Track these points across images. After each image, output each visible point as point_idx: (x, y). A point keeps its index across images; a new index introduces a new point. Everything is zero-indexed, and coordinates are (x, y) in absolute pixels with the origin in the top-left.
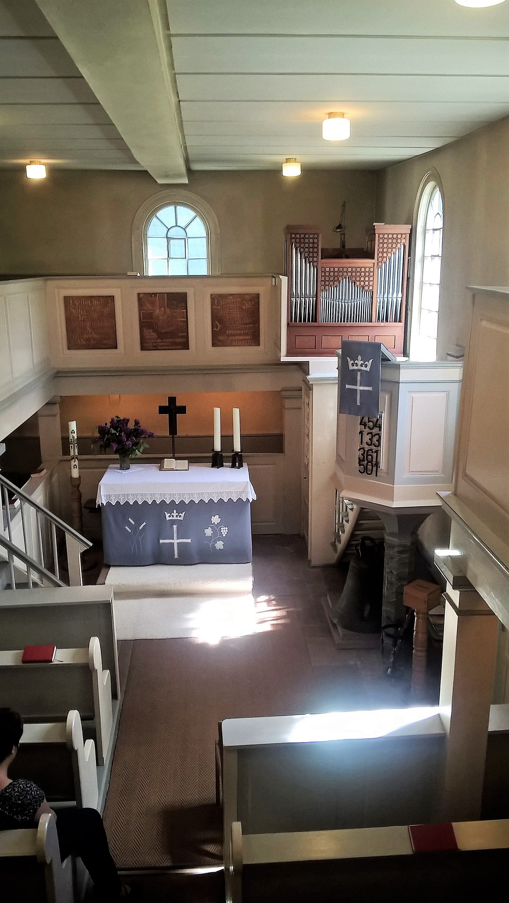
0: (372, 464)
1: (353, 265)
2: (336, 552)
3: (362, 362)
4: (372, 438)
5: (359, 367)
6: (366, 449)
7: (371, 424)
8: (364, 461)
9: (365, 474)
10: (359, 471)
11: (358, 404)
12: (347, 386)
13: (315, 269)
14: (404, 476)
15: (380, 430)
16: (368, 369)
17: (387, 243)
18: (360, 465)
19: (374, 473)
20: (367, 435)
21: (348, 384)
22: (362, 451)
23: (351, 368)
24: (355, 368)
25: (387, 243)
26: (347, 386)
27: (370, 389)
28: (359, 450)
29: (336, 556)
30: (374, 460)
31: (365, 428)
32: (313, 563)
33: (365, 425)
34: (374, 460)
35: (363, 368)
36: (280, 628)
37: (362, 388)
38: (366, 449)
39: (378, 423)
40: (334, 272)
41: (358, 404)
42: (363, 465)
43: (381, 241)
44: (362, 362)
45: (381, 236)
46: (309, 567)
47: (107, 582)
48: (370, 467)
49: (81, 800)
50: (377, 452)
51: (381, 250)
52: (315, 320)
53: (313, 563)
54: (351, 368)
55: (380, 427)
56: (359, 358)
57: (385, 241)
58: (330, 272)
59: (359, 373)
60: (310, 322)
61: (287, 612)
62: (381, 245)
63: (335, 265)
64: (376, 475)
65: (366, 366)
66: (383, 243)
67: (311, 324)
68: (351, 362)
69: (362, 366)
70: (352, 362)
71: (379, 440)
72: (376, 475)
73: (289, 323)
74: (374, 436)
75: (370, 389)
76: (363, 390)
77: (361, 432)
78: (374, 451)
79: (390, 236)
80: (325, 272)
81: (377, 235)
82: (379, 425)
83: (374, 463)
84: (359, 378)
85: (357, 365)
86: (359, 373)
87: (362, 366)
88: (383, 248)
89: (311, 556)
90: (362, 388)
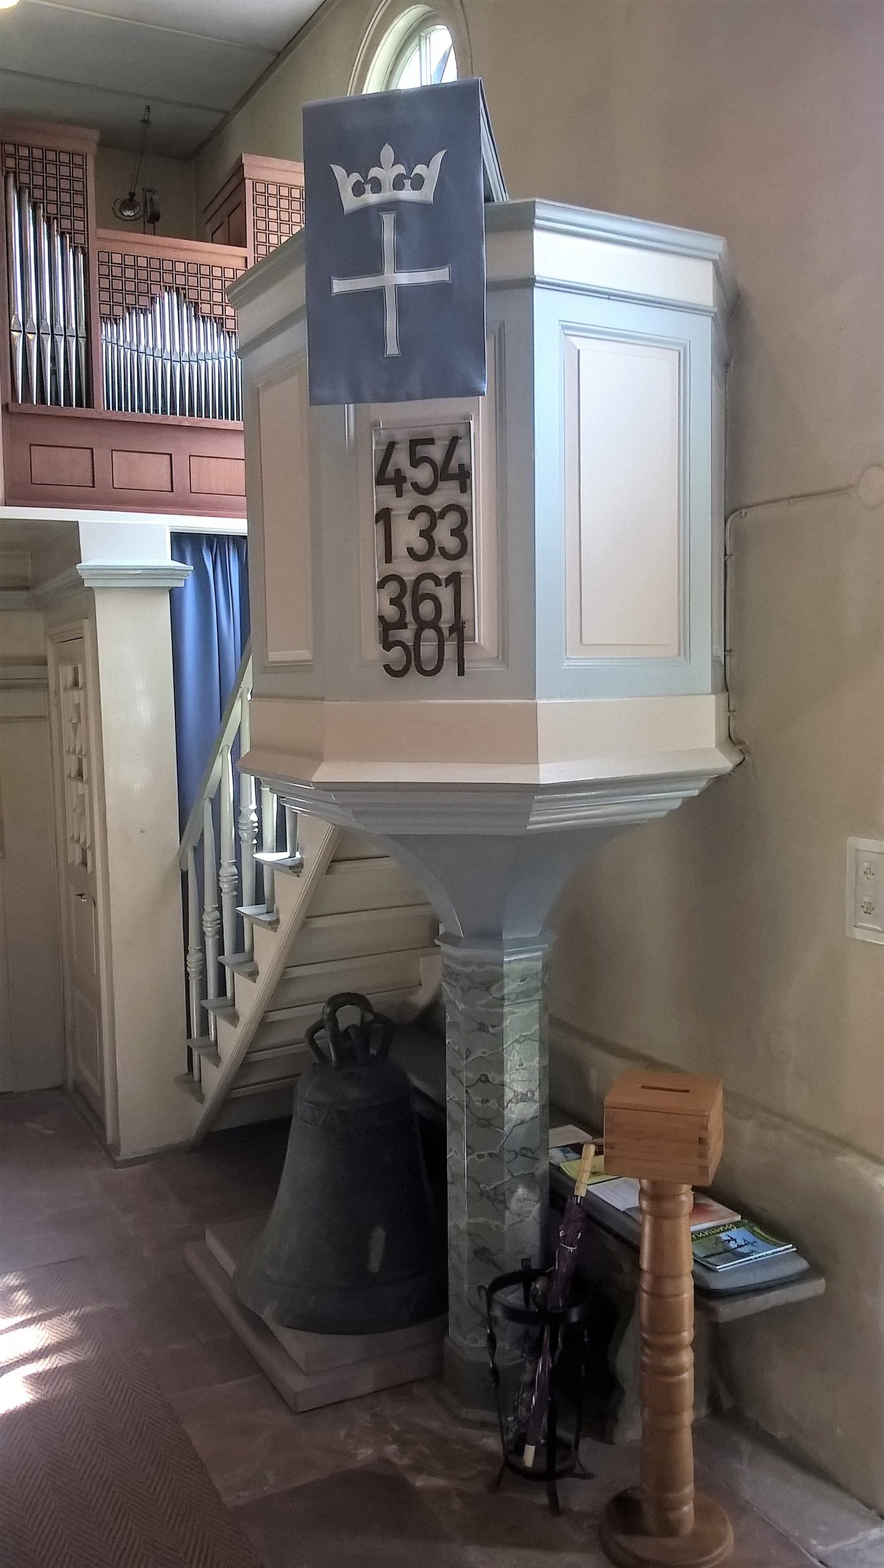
0: (439, 631)
1: (189, 257)
2: (201, 1100)
3: (401, 169)
4: (433, 525)
5: (388, 194)
6: (409, 579)
7: (423, 475)
8: (405, 626)
9: (413, 674)
10: (387, 668)
11: (392, 349)
12: (339, 286)
13: (81, 257)
14: (566, 662)
15: (465, 487)
16: (426, 194)
17: (278, 208)
18: (387, 645)
19: (450, 667)
20: (412, 516)
21: (344, 275)
22: (393, 588)
23: (350, 202)
24: (371, 198)
25: (278, 208)
26: (339, 286)
27: (442, 275)
28: (381, 585)
29: (199, 1113)
30: (447, 615)
31: (399, 494)
32: (126, 1152)
33: (398, 481)
34: (447, 615)
35: (407, 194)
36: (67, 1385)
37: (404, 278)
38: (409, 579)
39: (460, 453)
40: (136, 267)
41: (392, 349)
42: (399, 643)
43: (261, 200)
44: (401, 169)
45: (260, 188)
46: (116, 1165)
47: (618, 1439)
48: (428, 649)
49: (220, 814)
50: (455, 579)
51: (261, 225)
52: (87, 398)
53: (126, 1152)
54: (350, 202)
55: (463, 477)
56: (387, 153)
57: (272, 202)
58: (123, 266)
59: (388, 220)
60: (71, 405)
61: (75, 1319)
62: (261, 212)
63: (136, 250)
64: (461, 672)
65: (418, 183)
66: (267, 207)
67: (74, 410)
68: (345, 180)
69: (398, 184)
70: (356, 177)
71: (461, 532)
72: (461, 672)
73: (7, 405)
74: (442, 515)
75: (442, 275)
76: (409, 287)
77: (384, 516)
78: (442, 577)
79: (284, 192)
80: (110, 263)
81: (248, 184)
82: (461, 466)
83: (445, 626)
84: (389, 236)
85: (377, 186)
86: (388, 220)
87: (398, 184)
88: (266, 219)
89: (117, 1131)
90: (404, 278)
